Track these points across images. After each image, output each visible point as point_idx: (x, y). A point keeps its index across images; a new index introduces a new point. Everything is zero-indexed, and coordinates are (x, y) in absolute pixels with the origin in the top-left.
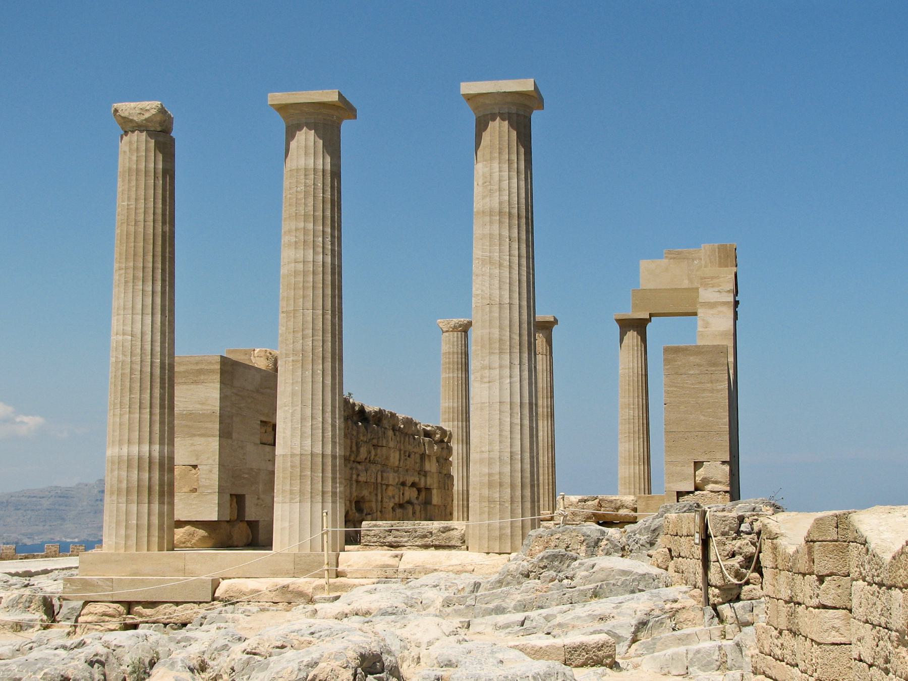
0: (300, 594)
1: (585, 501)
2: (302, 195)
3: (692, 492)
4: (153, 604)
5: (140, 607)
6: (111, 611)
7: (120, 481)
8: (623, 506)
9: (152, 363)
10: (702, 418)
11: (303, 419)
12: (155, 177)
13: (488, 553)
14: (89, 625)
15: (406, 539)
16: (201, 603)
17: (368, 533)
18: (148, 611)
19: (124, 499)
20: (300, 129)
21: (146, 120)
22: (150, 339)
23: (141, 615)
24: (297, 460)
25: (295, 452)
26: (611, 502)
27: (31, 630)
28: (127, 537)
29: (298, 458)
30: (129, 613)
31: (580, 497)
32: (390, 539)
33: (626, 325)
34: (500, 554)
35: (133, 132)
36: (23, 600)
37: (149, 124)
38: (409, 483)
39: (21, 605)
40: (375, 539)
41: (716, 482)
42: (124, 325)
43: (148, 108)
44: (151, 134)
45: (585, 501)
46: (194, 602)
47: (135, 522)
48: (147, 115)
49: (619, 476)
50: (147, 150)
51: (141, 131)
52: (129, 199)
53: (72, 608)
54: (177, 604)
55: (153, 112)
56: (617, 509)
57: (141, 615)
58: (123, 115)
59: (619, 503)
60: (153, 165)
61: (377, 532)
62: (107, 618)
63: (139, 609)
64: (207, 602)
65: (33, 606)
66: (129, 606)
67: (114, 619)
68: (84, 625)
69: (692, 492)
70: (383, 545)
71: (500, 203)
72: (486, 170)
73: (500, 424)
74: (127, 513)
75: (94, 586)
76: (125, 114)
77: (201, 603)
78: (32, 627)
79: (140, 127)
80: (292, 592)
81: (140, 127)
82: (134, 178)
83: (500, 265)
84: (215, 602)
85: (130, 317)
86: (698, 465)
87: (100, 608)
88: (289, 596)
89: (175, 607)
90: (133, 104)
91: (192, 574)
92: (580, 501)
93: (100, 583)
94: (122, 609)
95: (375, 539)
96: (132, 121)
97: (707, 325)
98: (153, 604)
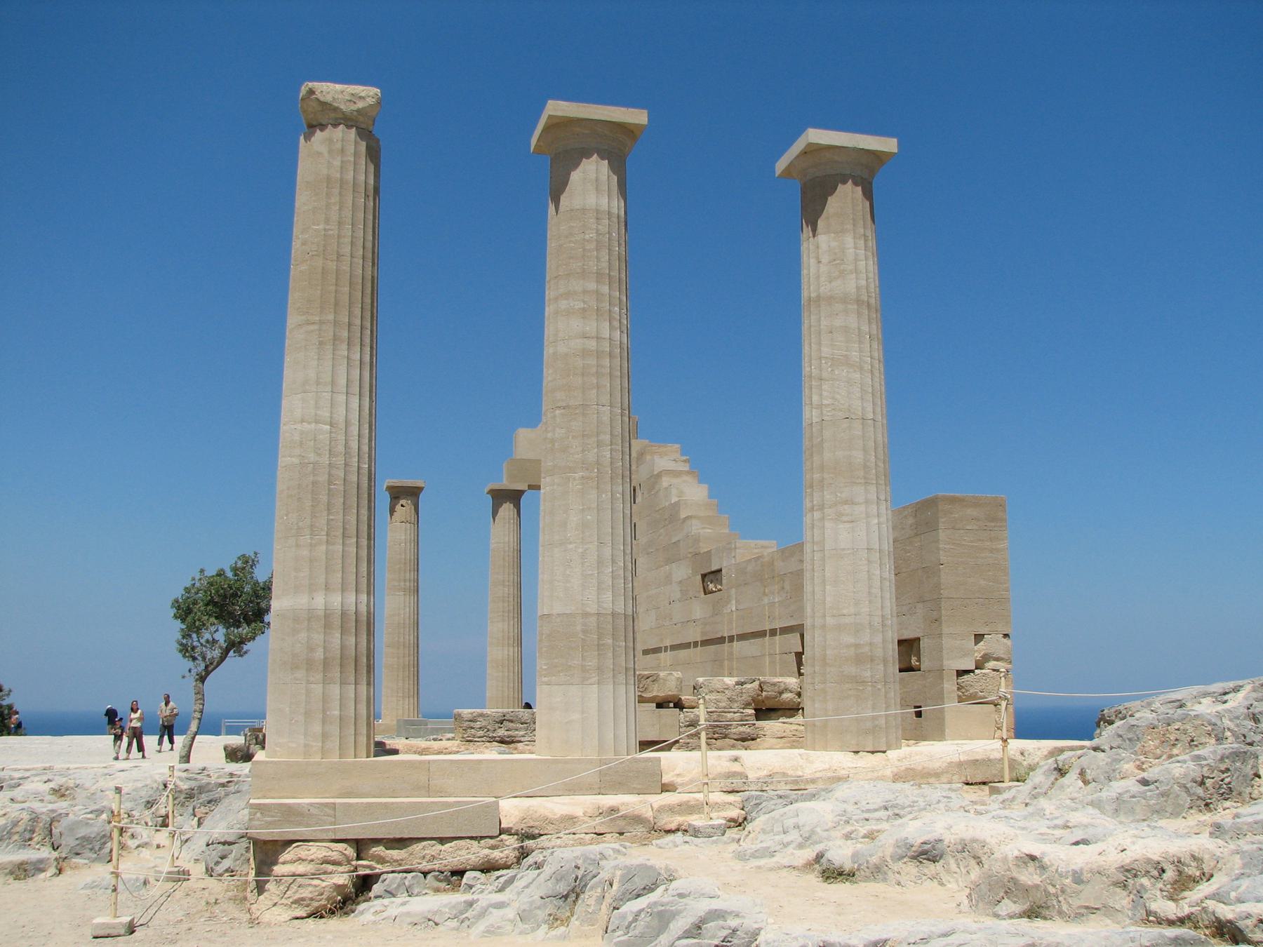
0: (637, 819)
1: (742, 684)
2: (593, 246)
3: (972, 671)
4: (400, 843)
5: (382, 848)
6: (335, 856)
7: (311, 649)
8: (786, 690)
9: (359, 467)
10: (983, 582)
11: (600, 563)
12: (367, 196)
13: (857, 752)
14: (299, 880)
15: (522, 733)
16: (482, 838)
17: (472, 724)
18: (395, 854)
19: (319, 676)
20: (589, 156)
21: (358, 111)
22: (356, 433)
23: (382, 860)
24: (593, 621)
25: (588, 610)
26: (774, 684)
27: (42, 875)
28: (325, 736)
29: (593, 620)
30: (359, 858)
31: (736, 679)
32: (501, 732)
33: (501, 497)
34: (873, 752)
35: (335, 125)
36: (20, 828)
37: (361, 119)
39: (16, 837)
40: (481, 733)
41: (997, 659)
42: (317, 407)
43: (363, 94)
44: (365, 134)
45: (742, 684)
46: (472, 838)
47: (337, 713)
48: (360, 105)
49: (489, 658)
50: (356, 154)
51: (349, 127)
52: (327, 221)
53: (83, 838)
54: (442, 840)
55: (371, 101)
56: (781, 693)
57: (382, 860)
58: (322, 99)
59: (783, 686)
60: (363, 178)
61: (484, 723)
62: (330, 868)
63: (379, 850)
64: (491, 837)
65: (37, 838)
66: (361, 846)
67: (340, 869)
68: (290, 879)
69: (972, 671)
70: (492, 740)
71: (858, 288)
72: (834, 244)
73: (870, 579)
74: (325, 699)
75: (301, 814)
76: (328, 99)
77: (482, 838)
78: (43, 870)
79: (348, 120)
80: (624, 817)
81: (348, 120)
82: (336, 191)
83: (861, 369)
84: (503, 836)
85: (327, 396)
86: (979, 638)
87: (316, 851)
88: (622, 823)
89: (439, 847)
90: (339, 87)
91: (441, 793)
92: (737, 683)
93: (313, 811)
95: (481, 733)
96: (336, 109)
98: (400, 843)
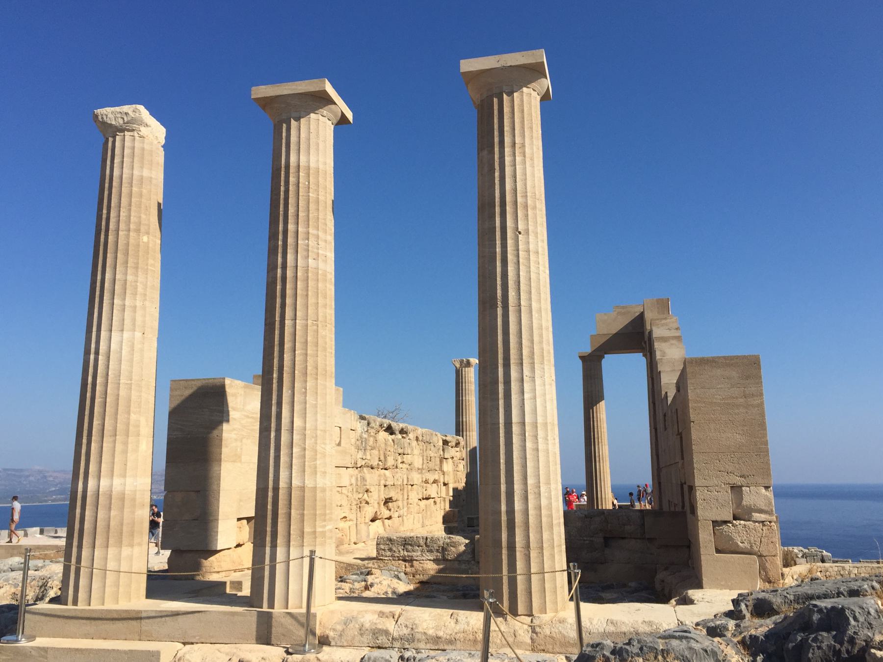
38: (431, 481)
90: (112, 109)
97: (664, 354)
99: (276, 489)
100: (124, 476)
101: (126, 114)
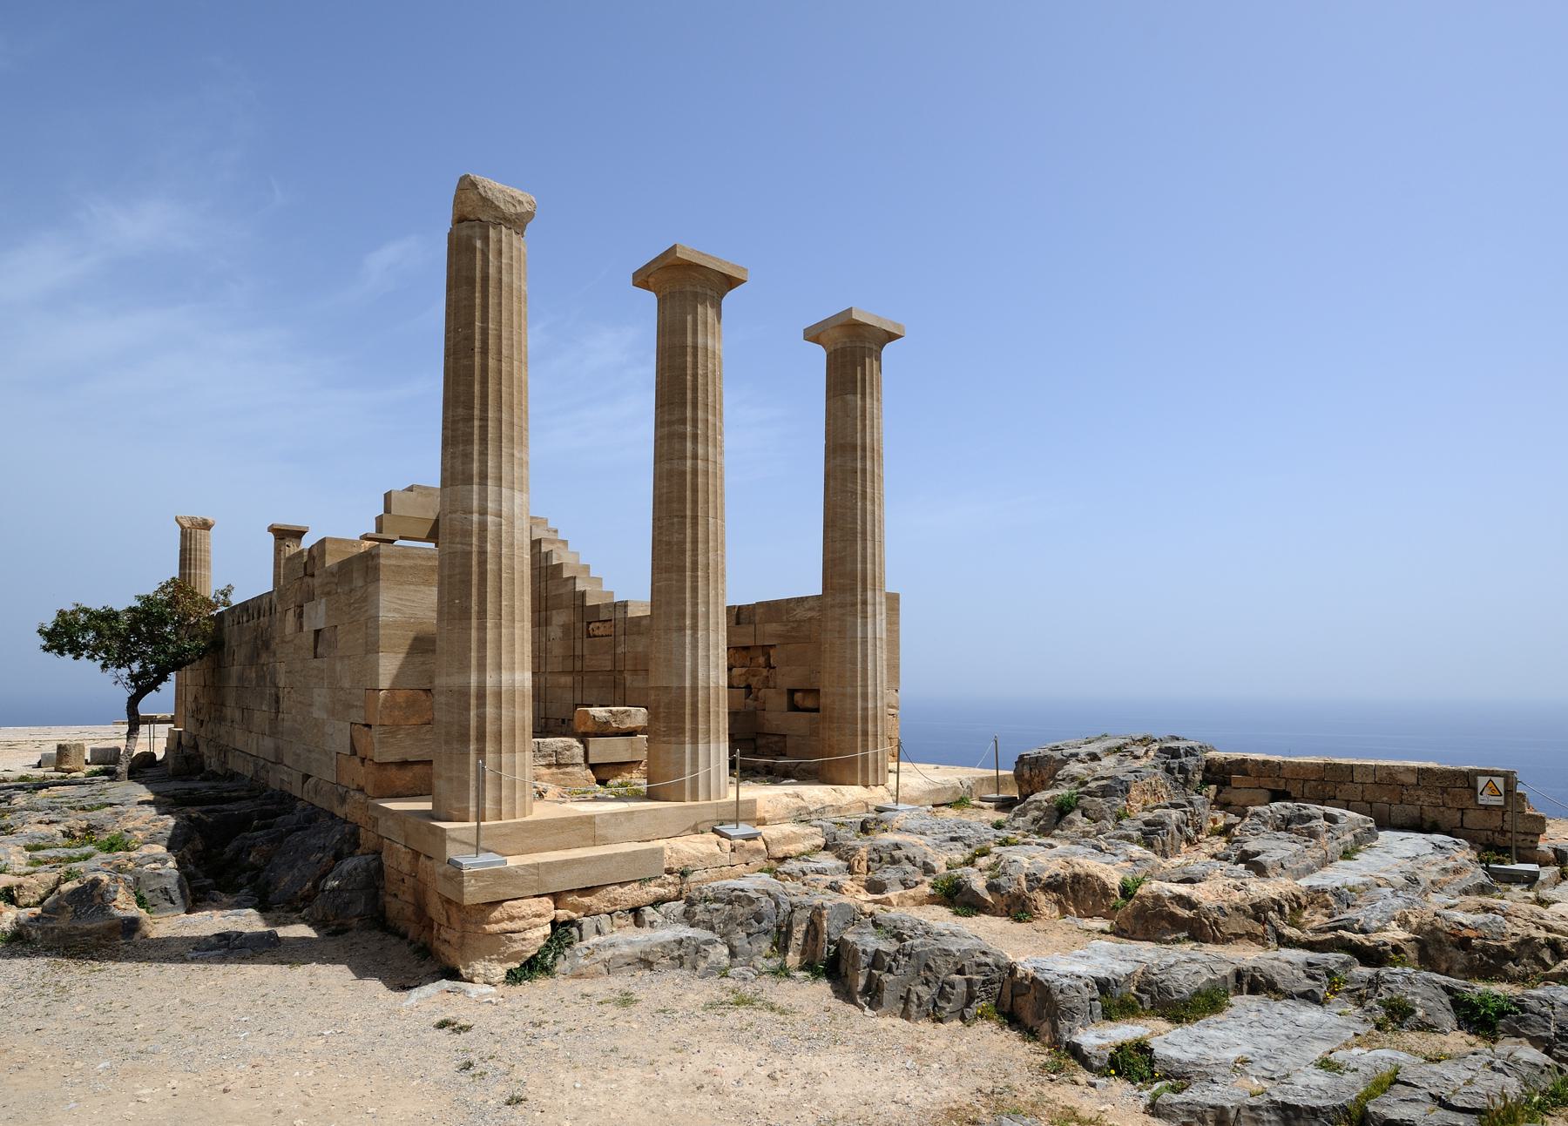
62: (537, 920)
94: (548, 903)
99: (695, 689)
100: (512, 669)
101: (520, 202)
